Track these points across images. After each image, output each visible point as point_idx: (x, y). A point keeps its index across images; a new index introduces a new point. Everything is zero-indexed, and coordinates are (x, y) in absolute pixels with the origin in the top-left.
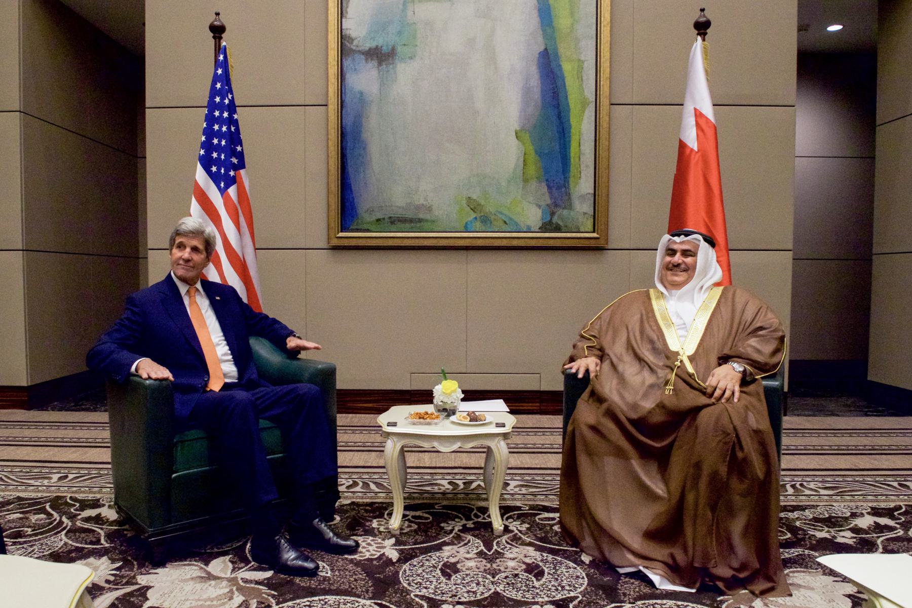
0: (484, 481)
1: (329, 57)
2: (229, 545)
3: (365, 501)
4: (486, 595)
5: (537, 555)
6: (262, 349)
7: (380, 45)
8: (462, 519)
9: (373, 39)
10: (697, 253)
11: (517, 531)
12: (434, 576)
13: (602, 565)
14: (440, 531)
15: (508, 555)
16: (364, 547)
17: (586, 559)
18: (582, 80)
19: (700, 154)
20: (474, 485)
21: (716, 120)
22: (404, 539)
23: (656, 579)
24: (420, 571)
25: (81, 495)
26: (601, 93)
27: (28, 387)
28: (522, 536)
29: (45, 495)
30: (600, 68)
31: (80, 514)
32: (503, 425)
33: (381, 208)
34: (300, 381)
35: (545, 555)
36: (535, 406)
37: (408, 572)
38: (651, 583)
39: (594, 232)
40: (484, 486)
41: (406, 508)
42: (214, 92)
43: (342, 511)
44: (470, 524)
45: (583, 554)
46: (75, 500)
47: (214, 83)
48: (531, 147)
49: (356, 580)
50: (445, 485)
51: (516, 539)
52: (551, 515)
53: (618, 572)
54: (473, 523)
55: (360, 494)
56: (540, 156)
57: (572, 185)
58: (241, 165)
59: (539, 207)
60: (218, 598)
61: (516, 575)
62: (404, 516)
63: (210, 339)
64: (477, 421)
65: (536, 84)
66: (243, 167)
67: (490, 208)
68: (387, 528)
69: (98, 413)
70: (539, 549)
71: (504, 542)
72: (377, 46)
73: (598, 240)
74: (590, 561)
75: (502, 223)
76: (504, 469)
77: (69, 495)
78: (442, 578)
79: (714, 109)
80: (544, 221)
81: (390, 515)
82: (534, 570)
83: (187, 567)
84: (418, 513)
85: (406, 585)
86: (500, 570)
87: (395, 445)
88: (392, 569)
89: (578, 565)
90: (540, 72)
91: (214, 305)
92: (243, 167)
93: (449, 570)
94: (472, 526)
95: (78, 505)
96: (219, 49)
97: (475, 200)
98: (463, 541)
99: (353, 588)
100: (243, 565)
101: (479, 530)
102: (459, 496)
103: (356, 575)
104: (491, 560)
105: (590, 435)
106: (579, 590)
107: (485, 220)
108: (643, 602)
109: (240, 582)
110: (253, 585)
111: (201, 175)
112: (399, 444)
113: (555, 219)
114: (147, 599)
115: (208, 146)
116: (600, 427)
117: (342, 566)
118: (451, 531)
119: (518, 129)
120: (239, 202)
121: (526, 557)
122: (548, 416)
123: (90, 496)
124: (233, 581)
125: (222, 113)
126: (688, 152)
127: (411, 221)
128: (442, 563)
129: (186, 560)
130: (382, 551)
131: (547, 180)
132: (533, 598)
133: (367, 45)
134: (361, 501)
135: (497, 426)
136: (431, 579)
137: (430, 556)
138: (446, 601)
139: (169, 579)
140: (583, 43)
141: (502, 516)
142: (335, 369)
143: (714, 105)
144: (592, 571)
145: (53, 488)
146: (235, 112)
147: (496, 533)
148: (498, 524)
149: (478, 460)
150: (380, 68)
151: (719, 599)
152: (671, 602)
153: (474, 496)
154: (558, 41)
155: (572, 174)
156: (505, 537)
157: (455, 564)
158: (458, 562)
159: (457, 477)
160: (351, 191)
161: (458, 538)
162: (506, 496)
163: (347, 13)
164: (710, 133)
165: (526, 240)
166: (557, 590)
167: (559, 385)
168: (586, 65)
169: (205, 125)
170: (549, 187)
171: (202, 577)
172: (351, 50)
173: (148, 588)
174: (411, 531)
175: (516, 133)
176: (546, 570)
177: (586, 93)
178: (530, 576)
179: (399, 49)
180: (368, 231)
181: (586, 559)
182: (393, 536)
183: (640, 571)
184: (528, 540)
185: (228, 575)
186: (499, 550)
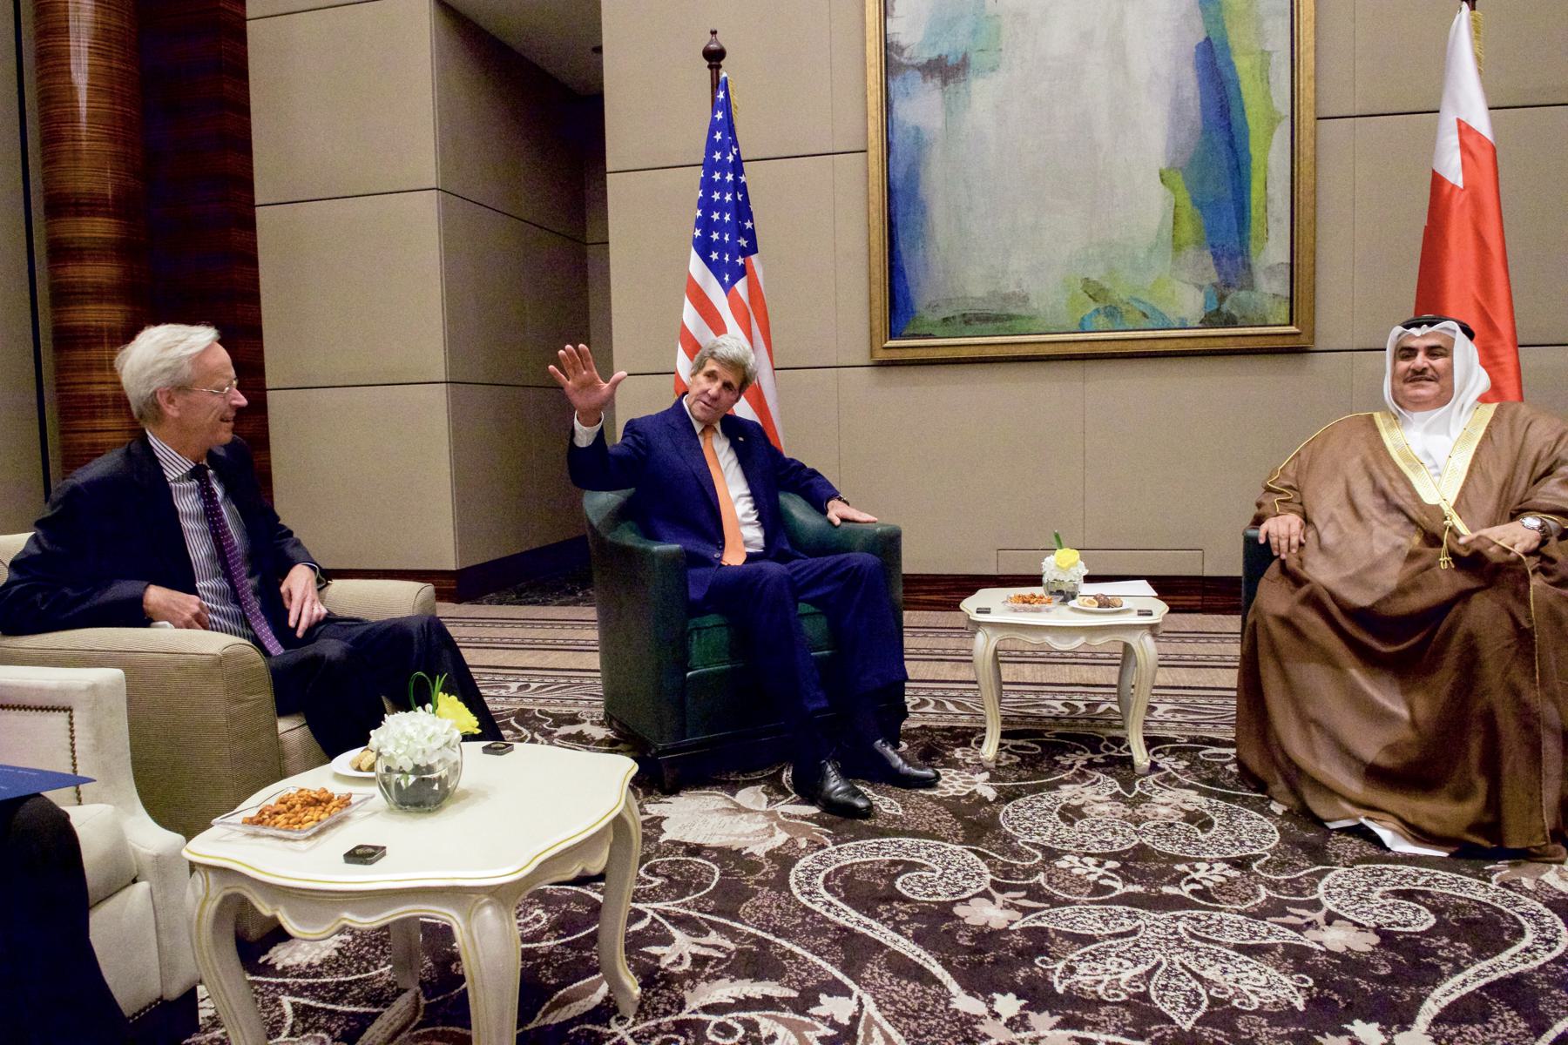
0: (1119, 703)
1: (868, 78)
2: (759, 773)
3: (941, 724)
4: (1127, 847)
5: (1203, 801)
6: (797, 509)
7: (944, 57)
8: (1085, 752)
9: (934, 45)
10: (1452, 350)
11: (1170, 770)
12: (1050, 821)
13: (1304, 815)
14: (1055, 765)
15: (1157, 799)
16: (945, 782)
17: (1278, 808)
18: (1268, 83)
19: (1467, 192)
20: (1102, 708)
21: (1495, 137)
22: (1002, 774)
23: (1386, 835)
24: (1028, 814)
25: (552, 708)
26: (1301, 102)
27: (457, 571)
28: (1179, 776)
29: (506, 707)
30: (1299, 61)
31: (556, 731)
32: (1149, 614)
33: (949, 301)
34: (849, 551)
35: (1214, 801)
36: (1195, 600)
37: (1011, 815)
38: (1378, 842)
39: (1291, 324)
40: (1118, 710)
41: (1004, 735)
42: (712, 146)
43: (910, 736)
44: (1098, 759)
45: (1274, 802)
46: (547, 714)
47: (712, 132)
48: (1187, 195)
49: (938, 821)
50: (1058, 707)
51: (1168, 779)
52: (1223, 751)
53: (1327, 828)
54: (1103, 758)
55: (933, 716)
56: (1201, 208)
57: (1253, 246)
58: (753, 249)
59: (1201, 288)
60: (756, 833)
61: (1171, 825)
62: (1001, 745)
63: (728, 494)
64: (1109, 607)
65: (1192, 95)
66: (755, 251)
67: (1120, 294)
68: (979, 760)
69: (552, 608)
70: (1202, 792)
71: (1152, 783)
72: (940, 56)
73: (1296, 337)
74: (1284, 812)
75: (1139, 316)
76: (1149, 688)
77: (537, 708)
78: (1061, 824)
79: (1491, 115)
80: (1208, 310)
81: (980, 743)
82: (1199, 820)
83: (708, 797)
84: (1020, 742)
85: (1010, 830)
86: (1146, 817)
87: (989, 640)
88: (988, 810)
89: (1266, 816)
90: (1198, 76)
91: (734, 445)
92: (755, 251)
93: (1071, 814)
94: (1102, 761)
95: (551, 720)
96: (717, 84)
97: (1094, 282)
98: (1090, 779)
99: (935, 831)
100: (781, 797)
101: (1112, 765)
102: (1080, 722)
103: (938, 814)
104: (1133, 804)
105: (1279, 633)
106: (1267, 847)
107: (1112, 312)
108: (1366, 866)
109: (781, 816)
110: (798, 821)
111: (696, 266)
112: (994, 638)
113: (1226, 307)
114: (663, 831)
115: (705, 224)
116: (1298, 622)
117: (918, 803)
118: (1071, 767)
119: (1164, 168)
120: (750, 302)
121: (1184, 802)
122: (1215, 616)
123: (564, 710)
124: (771, 815)
125: (723, 176)
126: (1447, 190)
127: (997, 318)
128: (1060, 805)
129: (704, 789)
130: (972, 788)
131: (1213, 246)
132: (1197, 854)
133: (926, 55)
134: (934, 724)
135: (1139, 615)
136: (1045, 825)
137: (1042, 796)
138: (1069, 851)
139: (686, 809)
140: (1268, 25)
141: (1148, 748)
142: (900, 532)
143: (1490, 109)
144: (1287, 824)
145: (514, 700)
146: (742, 172)
147: (1138, 771)
148: (1141, 757)
149: (1110, 675)
150: (946, 89)
151: (1486, 868)
152: (1410, 868)
153: (1103, 723)
154: (1228, 25)
155: (1253, 233)
156: (1153, 777)
157: (1079, 808)
158: (1083, 805)
159: (1075, 697)
160: (904, 277)
161: (1082, 775)
162: (1151, 724)
163: (893, 9)
164: (1485, 158)
165: (1178, 341)
166: (1233, 845)
167: (1234, 567)
168: (1274, 58)
169: (700, 195)
170: (1215, 255)
171: (730, 810)
172: (900, 65)
173: (663, 819)
174: (1012, 764)
175: (1161, 175)
176: (1216, 821)
177: (1275, 104)
178: (1191, 826)
179: (974, 58)
180: (930, 336)
181: (1278, 808)
182: (985, 770)
183: (1362, 825)
184: (1188, 781)
185: (764, 808)
186: (1144, 792)
